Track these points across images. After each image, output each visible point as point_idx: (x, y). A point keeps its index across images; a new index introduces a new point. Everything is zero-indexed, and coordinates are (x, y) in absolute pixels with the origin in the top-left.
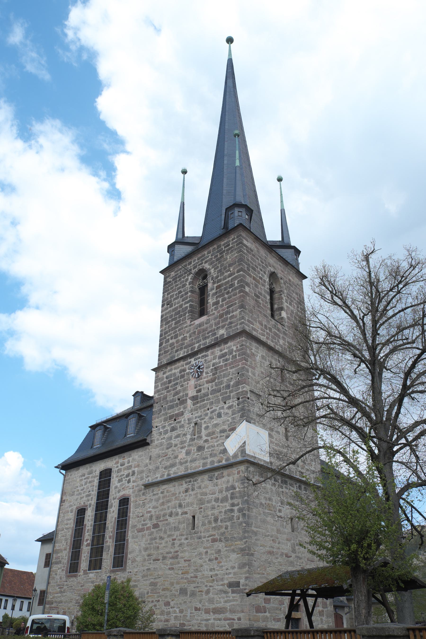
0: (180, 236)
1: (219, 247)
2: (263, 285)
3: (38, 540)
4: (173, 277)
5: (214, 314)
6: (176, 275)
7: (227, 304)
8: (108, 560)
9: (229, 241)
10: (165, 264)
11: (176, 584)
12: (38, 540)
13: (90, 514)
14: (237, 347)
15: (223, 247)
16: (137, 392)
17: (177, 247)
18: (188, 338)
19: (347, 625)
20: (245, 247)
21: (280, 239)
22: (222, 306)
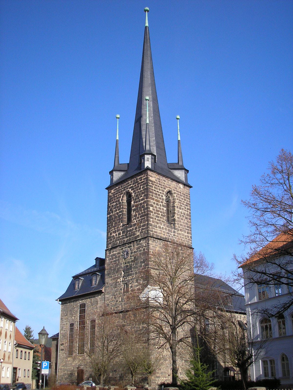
0: (116, 164)
1: (137, 179)
2: (162, 202)
3: (72, 277)
4: (113, 193)
5: (134, 222)
6: (114, 192)
7: (141, 217)
8: (146, 193)
9: (142, 177)
10: (108, 184)
11: (185, 221)
12: (72, 277)
13: (77, 326)
14: (145, 244)
15: (139, 180)
16: (97, 258)
17: (114, 173)
18: (121, 234)
19: (257, 301)
20: (150, 182)
21: (177, 162)
22: (138, 218)
